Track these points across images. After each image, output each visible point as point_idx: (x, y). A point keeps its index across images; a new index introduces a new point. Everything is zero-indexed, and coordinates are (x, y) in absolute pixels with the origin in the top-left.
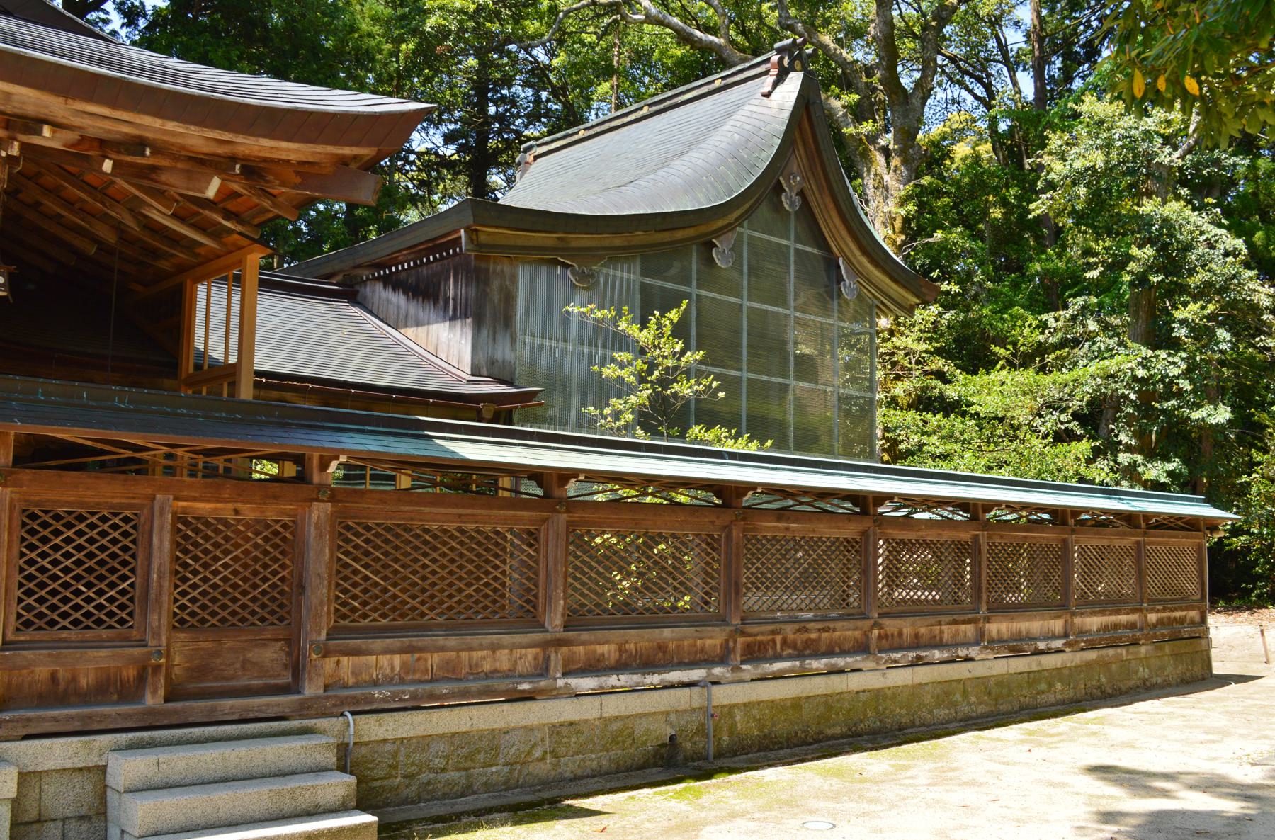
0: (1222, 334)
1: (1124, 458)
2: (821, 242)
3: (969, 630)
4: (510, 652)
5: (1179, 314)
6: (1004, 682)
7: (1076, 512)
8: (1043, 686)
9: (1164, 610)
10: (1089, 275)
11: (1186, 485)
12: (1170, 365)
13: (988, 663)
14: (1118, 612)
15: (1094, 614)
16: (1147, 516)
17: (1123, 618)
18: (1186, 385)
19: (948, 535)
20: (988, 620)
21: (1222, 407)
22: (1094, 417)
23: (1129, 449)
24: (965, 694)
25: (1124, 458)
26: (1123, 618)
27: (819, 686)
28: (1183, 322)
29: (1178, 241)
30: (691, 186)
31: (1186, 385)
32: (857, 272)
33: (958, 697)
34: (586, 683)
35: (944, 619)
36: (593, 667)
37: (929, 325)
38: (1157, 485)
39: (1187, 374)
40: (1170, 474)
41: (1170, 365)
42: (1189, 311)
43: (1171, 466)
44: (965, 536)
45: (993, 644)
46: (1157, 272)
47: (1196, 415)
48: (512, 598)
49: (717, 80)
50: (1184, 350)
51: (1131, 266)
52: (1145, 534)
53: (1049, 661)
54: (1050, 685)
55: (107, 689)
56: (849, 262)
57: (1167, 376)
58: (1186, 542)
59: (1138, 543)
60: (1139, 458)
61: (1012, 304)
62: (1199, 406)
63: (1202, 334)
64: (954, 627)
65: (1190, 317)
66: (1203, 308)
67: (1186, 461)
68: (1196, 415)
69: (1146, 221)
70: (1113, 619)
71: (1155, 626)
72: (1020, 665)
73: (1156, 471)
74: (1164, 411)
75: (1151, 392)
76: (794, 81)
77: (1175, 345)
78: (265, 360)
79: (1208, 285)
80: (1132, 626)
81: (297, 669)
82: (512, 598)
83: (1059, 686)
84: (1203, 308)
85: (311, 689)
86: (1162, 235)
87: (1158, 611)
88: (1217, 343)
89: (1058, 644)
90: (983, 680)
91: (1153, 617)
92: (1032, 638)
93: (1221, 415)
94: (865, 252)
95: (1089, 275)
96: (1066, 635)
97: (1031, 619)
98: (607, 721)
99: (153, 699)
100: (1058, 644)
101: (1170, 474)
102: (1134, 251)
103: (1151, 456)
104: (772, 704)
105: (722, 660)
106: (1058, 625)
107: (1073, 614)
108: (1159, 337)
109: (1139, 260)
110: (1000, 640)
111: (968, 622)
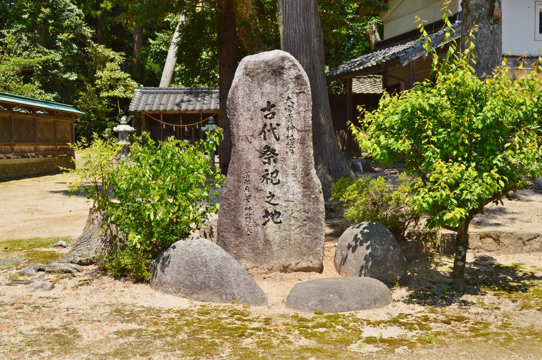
0: (75, 46)
3: (8, 147)
6: (20, 166)
8: (30, 168)
9: (62, 145)
10: (24, 16)
12: (56, 56)
13: (15, 160)
14: (49, 145)
15: (43, 145)
16: (58, 111)
17: (50, 147)
18: (61, 64)
20: (15, 145)
21: (74, 74)
24: (9, 169)
26: (50, 147)
28: (61, 40)
29: (59, 8)
33: (7, 170)
35: (3, 144)
40: (54, 98)
41: (56, 56)
42: (64, 36)
43: (54, 95)
45: (16, 153)
46: (51, 19)
47: (65, 76)
48: (482, 77)
50: (61, 51)
51: (41, 15)
52: (57, 118)
53: (32, 160)
54: (32, 168)
57: (55, 60)
58: (68, 122)
59: (54, 121)
62: (65, 73)
63: (66, 43)
64: (5, 147)
65: (64, 38)
66: (69, 35)
68: (65, 76)
70: (47, 147)
71: (59, 150)
72: (23, 161)
74: (52, 74)
75: (47, 66)
77: (57, 49)
79: (69, 26)
80: (53, 150)
82: (482, 77)
83: (34, 169)
84: (69, 35)
86: (53, 4)
87: (60, 145)
88: (73, 49)
89: (33, 154)
90: (13, 165)
91: (59, 147)
92: (26, 152)
93: (74, 77)
95: (24, 16)
96: (35, 152)
97: (26, 145)
100: (33, 154)
101: (54, 98)
102: (43, 9)
106: (32, 148)
107: (37, 145)
108: (51, 44)
109: (44, 13)
110: (17, 152)
111: (8, 145)
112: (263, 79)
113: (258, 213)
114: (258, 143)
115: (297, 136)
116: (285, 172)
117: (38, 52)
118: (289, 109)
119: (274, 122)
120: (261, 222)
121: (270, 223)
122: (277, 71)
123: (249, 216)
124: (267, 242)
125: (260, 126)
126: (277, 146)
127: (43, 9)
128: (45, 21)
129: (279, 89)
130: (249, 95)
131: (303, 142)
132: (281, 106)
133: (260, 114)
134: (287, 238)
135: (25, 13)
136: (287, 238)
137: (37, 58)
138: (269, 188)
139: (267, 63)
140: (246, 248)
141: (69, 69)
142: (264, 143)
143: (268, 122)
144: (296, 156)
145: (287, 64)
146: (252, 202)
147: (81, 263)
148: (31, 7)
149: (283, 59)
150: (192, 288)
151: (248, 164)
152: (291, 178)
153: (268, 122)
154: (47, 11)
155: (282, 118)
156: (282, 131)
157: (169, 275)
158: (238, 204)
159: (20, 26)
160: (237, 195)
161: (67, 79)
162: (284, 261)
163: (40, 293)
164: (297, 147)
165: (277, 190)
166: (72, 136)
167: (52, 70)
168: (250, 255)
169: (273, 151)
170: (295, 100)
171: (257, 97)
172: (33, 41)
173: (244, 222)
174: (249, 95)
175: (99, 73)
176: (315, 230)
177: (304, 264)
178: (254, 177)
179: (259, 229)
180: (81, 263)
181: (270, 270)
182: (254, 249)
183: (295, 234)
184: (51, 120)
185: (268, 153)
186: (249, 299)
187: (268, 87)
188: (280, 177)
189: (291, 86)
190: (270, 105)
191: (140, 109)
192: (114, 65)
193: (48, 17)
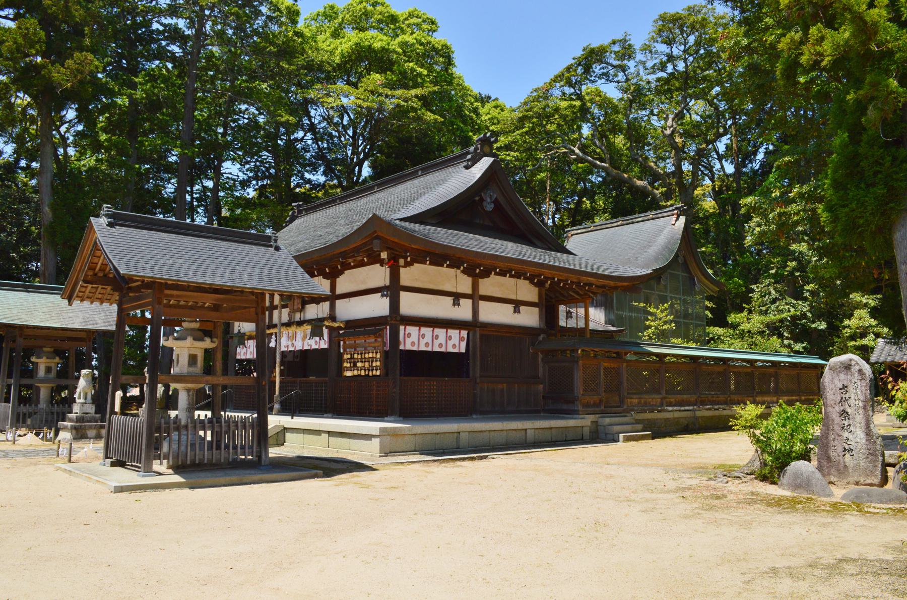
1: (786, 342)
2: (690, 273)
4: (655, 399)
5: (807, 288)
7: (780, 362)
11: (808, 352)
12: (804, 307)
16: (801, 363)
18: (809, 314)
19: (745, 370)
22: (774, 329)
23: (787, 338)
25: (786, 342)
27: (717, 413)
28: (808, 291)
30: (656, 259)
31: (809, 314)
32: (700, 281)
34: (670, 408)
36: (670, 405)
37: (198, 107)
38: (797, 352)
39: (810, 311)
41: (804, 307)
44: (749, 370)
46: (798, 271)
49: (651, 214)
51: (788, 269)
55: (596, 405)
56: (698, 278)
60: (792, 342)
61: (733, 277)
62: (814, 322)
63: (813, 293)
67: (809, 343)
69: (794, 252)
73: (798, 347)
76: (682, 219)
77: (806, 299)
78: (591, 328)
81: (622, 402)
85: (625, 407)
93: (823, 326)
94: (703, 275)
98: (675, 418)
99: (603, 408)
101: (804, 348)
103: (796, 341)
104: (707, 417)
105: (695, 405)
108: (798, 295)
112: (840, 372)
113: (840, 449)
114: (838, 408)
115: (861, 404)
116: (854, 425)
117: (787, 304)
118: (856, 388)
119: (847, 396)
120: (842, 454)
121: (848, 455)
122: (847, 367)
123: (834, 451)
124: (845, 466)
125: (839, 398)
126: (849, 410)
127: (789, 263)
128: (792, 273)
129: (849, 377)
130: (832, 381)
131: (865, 408)
132: (851, 387)
133: (839, 391)
134: (858, 465)
135: (772, 268)
136: (858, 465)
137: (790, 308)
138: (846, 434)
139: (841, 363)
140: (833, 469)
141: (817, 317)
142: (842, 408)
143: (844, 396)
144: (861, 416)
145: (853, 363)
146: (836, 443)
147: (747, 474)
148: (778, 262)
149: (851, 360)
150: (796, 487)
151: (833, 420)
152: (858, 429)
153: (844, 396)
154: (793, 264)
155: (852, 393)
156: (852, 401)
157: (785, 479)
158: (828, 443)
159: (767, 281)
160: (827, 438)
161: (816, 328)
162: (856, 479)
163: (720, 484)
164: (861, 410)
165: (851, 436)
166: (460, 459)
167: (801, 320)
168: (836, 473)
169: (847, 413)
170: (859, 383)
171: (836, 382)
172: (782, 294)
173: (832, 454)
174: (832, 381)
175: (847, 322)
176: (875, 461)
177: (868, 481)
178: (837, 428)
179: (841, 458)
180: (747, 474)
181: (848, 483)
182: (838, 470)
183: (863, 463)
184: (794, 372)
185: (844, 414)
186: (821, 493)
187: (842, 376)
188: (852, 428)
189: (856, 375)
190: (844, 387)
191: (882, 359)
192: (864, 313)
193: (795, 269)
